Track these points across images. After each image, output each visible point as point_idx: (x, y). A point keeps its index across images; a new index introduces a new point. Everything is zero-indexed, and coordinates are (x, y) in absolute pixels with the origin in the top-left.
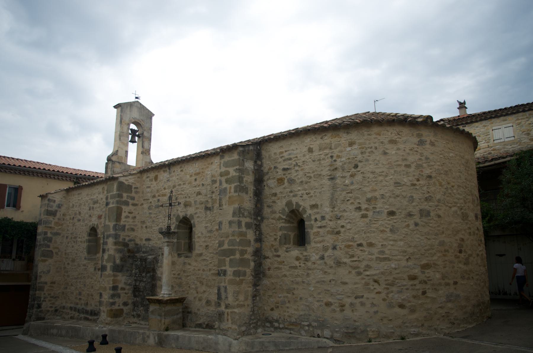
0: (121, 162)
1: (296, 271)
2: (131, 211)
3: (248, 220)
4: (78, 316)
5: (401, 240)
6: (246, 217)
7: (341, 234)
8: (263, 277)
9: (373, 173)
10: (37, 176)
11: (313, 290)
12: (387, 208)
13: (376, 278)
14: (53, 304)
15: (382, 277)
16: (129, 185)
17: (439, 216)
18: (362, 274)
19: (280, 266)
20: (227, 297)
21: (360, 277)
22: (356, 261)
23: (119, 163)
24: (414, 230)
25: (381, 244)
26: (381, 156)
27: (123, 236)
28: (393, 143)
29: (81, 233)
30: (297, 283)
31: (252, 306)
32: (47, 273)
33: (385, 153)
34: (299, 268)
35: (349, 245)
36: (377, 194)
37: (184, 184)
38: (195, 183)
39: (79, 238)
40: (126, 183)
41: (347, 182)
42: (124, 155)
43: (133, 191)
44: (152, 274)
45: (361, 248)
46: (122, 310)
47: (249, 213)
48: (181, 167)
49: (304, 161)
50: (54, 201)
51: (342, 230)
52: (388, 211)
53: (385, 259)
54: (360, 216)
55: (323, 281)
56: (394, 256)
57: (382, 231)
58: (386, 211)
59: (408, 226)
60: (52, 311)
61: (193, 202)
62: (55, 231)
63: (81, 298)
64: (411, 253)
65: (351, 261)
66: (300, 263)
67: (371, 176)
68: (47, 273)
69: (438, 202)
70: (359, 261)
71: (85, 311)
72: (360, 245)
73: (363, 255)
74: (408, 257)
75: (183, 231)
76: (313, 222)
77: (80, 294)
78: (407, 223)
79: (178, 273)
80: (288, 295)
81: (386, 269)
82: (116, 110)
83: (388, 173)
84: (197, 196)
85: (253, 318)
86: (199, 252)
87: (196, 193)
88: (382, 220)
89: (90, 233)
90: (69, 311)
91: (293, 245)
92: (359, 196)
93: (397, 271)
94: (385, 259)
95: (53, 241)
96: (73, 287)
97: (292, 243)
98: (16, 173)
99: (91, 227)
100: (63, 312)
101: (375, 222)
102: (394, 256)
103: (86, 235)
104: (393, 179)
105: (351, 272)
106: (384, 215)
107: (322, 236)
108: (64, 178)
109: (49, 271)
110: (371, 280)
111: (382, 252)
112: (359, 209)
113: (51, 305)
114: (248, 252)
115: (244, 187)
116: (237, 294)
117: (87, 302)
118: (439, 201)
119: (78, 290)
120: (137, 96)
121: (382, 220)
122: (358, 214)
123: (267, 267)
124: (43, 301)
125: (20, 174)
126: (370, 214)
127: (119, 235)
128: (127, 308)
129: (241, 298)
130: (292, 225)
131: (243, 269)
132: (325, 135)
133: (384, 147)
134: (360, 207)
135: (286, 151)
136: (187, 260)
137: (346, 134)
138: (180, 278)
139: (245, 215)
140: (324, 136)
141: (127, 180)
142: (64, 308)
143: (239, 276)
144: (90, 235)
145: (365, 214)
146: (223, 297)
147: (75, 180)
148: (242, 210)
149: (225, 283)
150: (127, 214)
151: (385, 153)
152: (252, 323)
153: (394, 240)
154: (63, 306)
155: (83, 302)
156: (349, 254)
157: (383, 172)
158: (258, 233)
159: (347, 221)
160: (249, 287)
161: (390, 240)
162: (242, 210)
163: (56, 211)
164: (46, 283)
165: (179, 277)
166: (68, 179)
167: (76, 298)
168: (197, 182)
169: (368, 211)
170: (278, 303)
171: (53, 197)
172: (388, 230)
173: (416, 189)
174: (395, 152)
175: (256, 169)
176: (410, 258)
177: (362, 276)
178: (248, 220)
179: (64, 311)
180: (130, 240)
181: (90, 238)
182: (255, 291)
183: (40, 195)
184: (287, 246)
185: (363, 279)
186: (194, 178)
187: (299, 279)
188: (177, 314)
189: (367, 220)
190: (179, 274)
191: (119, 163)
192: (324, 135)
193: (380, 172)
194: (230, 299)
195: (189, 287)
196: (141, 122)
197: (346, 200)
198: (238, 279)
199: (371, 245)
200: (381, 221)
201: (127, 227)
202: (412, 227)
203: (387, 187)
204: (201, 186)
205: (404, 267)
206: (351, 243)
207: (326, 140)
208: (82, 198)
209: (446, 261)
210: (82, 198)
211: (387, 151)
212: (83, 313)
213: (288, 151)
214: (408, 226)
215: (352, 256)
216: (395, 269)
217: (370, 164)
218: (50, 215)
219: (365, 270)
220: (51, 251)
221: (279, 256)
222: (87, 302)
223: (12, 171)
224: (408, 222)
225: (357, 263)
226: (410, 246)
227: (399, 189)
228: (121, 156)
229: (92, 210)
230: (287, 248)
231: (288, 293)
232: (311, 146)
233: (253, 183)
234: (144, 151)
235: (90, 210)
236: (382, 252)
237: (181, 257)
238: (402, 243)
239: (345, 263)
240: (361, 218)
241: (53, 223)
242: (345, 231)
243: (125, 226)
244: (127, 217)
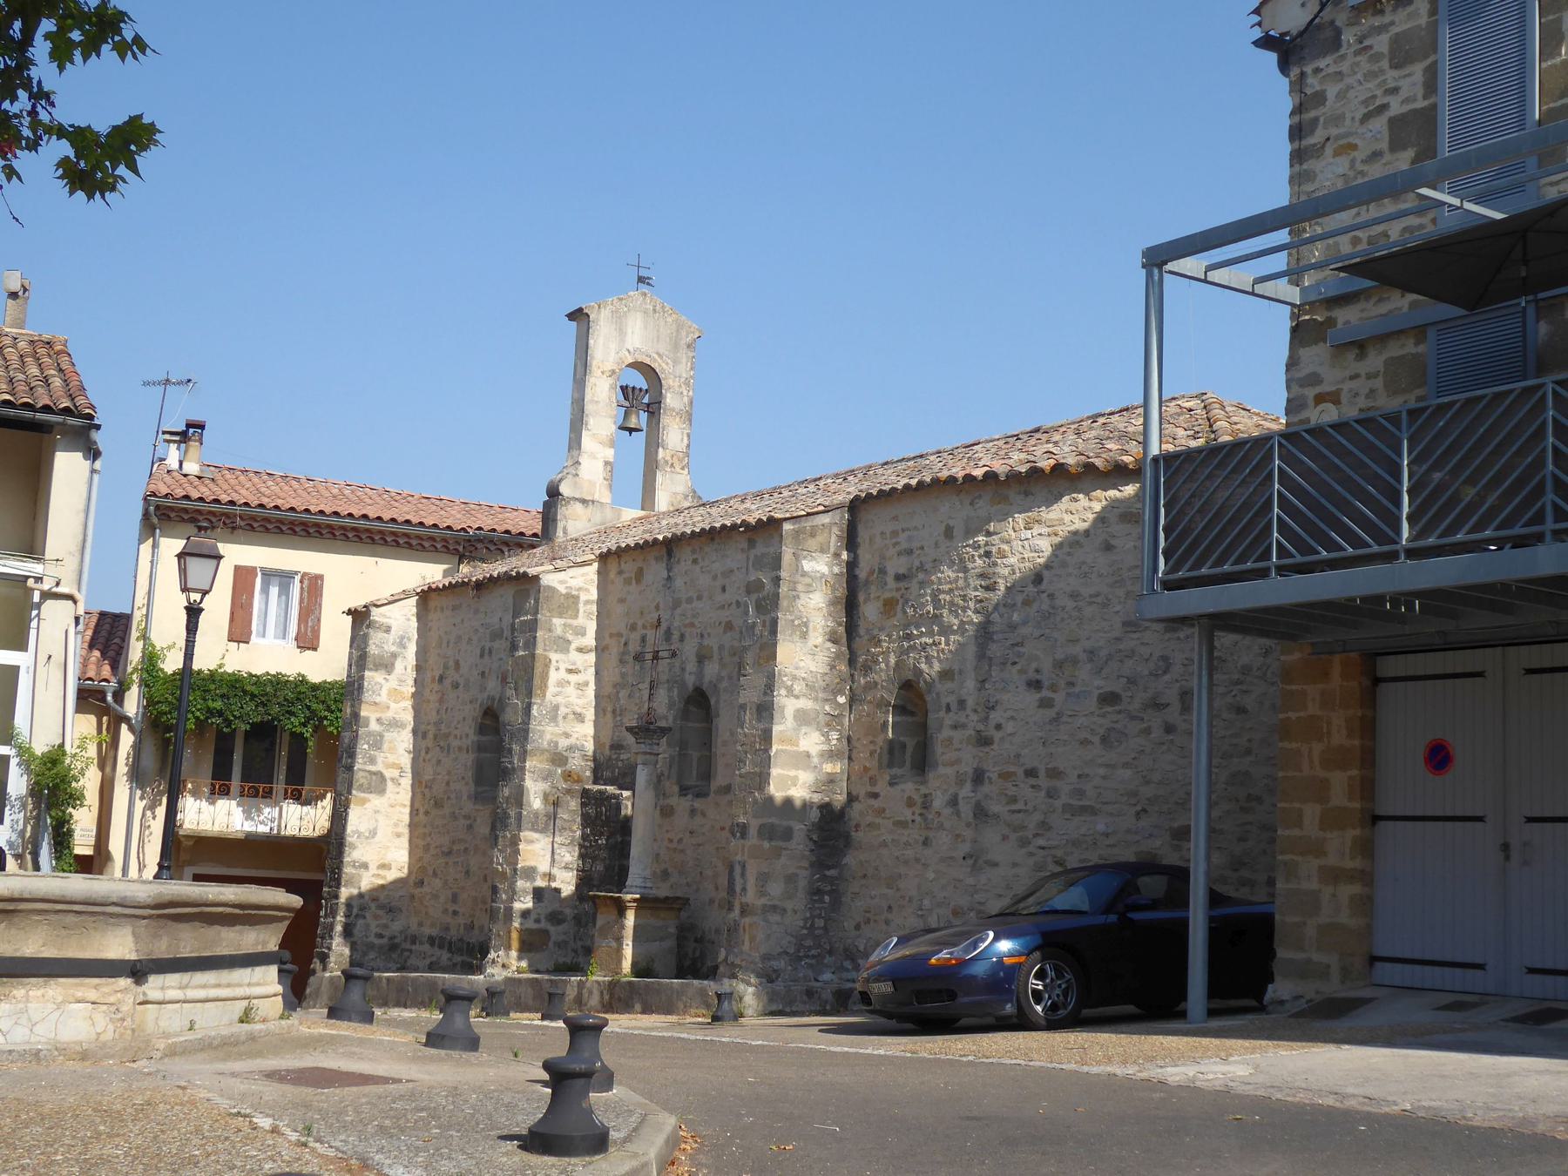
0: (590, 498)
1: (906, 832)
2: (573, 667)
3: (805, 704)
4: (450, 959)
5: (1126, 765)
6: (797, 697)
7: (995, 746)
8: (845, 846)
9: (1074, 596)
10: (343, 537)
11: (934, 879)
12: (1100, 684)
13: (1059, 853)
14: (386, 926)
15: (1072, 853)
16: (568, 596)
17: (1241, 710)
18: (1030, 843)
19: (877, 820)
20: (744, 889)
21: (1024, 851)
22: (1019, 811)
23: (584, 502)
24: (1163, 744)
25: (1076, 773)
26: (1097, 555)
27: (552, 734)
28: (1130, 521)
29: (459, 722)
30: (906, 862)
31: (808, 915)
32: (367, 838)
33: (1108, 547)
34: (910, 825)
35: (1008, 772)
36: (1076, 650)
37: (700, 598)
38: (720, 598)
39: (456, 736)
40: (562, 589)
41: (1016, 617)
42: (601, 477)
43: (581, 611)
44: (620, 839)
45: (1032, 781)
46: (545, 932)
47: (807, 685)
48: (694, 551)
49: (935, 560)
50: (388, 630)
51: (997, 735)
52: (1101, 694)
53: (1084, 810)
54: (1037, 704)
55: (951, 858)
56: (1106, 803)
57: (1085, 742)
58: (1097, 693)
59: (1147, 731)
60: (381, 947)
61: (715, 649)
62: (389, 715)
63: (457, 909)
64: (1148, 799)
65: (1009, 811)
66: (913, 814)
67: (1070, 604)
68: (367, 838)
69: (1244, 674)
70: (1026, 811)
71: (465, 947)
72: (1031, 773)
73: (1036, 797)
74: (1139, 808)
75: (697, 725)
76: (942, 714)
77: (455, 898)
78: (1145, 725)
79: (678, 837)
80: (889, 891)
81: (1084, 835)
82: (574, 324)
83: (1110, 597)
84: (725, 632)
85: (808, 943)
86: (724, 784)
87: (723, 624)
88: (1086, 715)
89: (481, 724)
90: (426, 947)
91: (912, 769)
92: (1038, 653)
93: (1111, 841)
94: (1084, 810)
95: (385, 746)
96: (437, 880)
97: (908, 764)
98: (282, 532)
99: (485, 707)
100: (411, 951)
101: (1070, 720)
102: (1106, 803)
103: (472, 731)
104: (1121, 614)
105: (1008, 837)
106: (1091, 704)
107: (956, 750)
108: (426, 544)
109: (373, 833)
110: (1049, 859)
111: (1080, 793)
112: (1035, 685)
113: (379, 931)
114: (801, 782)
115: (796, 623)
116: (763, 878)
117: (472, 922)
118: (1246, 670)
119: (451, 888)
120: (643, 273)
121: (1086, 715)
122: (1033, 698)
123: (853, 823)
124: (357, 916)
125: (295, 533)
126: (1059, 698)
127: (539, 731)
128: (561, 928)
129: (776, 889)
130: (910, 719)
131: (785, 823)
132: (980, 497)
133: (1107, 532)
134: (1038, 682)
135: (903, 530)
136: (698, 804)
137: (1022, 497)
138: (682, 851)
139: (796, 692)
140: (976, 498)
141: (562, 582)
142: (414, 940)
143: (771, 839)
144: (482, 730)
145: (1049, 698)
146: (738, 889)
147: (461, 549)
148: (785, 679)
149: (743, 855)
150: (562, 674)
151: (1108, 547)
152: (807, 957)
153: (1107, 766)
154: (412, 936)
155: (462, 922)
156: (1006, 795)
157: (1097, 595)
158: (836, 737)
159: (1009, 713)
160: (800, 867)
161: (1101, 765)
162: (785, 679)
163: (394, 656)
164: (365, 866)
165: (680, 847)
166: (439, 546)
167: (445, 911)
168: (727, 596)
169: (1055, 691)
170: (869, 912)
171: (385, 616)
172: (1096, 740)
173: (1179, 639)
174: (1132, 544)
175: (837, 574)
176: (1144, 810)
177: (1031, 848)
178: (805, 704)
179: (414, 947)
180: (570, 748)
181: (484, 738)
182: (819, 880)
183: (349, 610)
184: (895, 771)
185: (1031, 854)
186: (719, 583)
187: (909, 853)
188: (662, 939)
189: (1051, 713)
190: (680, 841)
191: (584, 502)
192: (977, 494)
193: (1091, 596)
194: (750, 897)
195: (701, 873)
196: (655, 360)
197: (1010, 662)
198: (766, 845)
199: (1055, 774)
200: (1084, 718)
201: (563, 711)
202: (1157, 733)
203: (1105, 632)
204: (734, 606)
205: (1128, 831)
206: (1012, 769)
207: (980, 508)
208: (463, 621)
209: (1251, 823)
210: (463, 621)
211: (1113, 542)
212: (460, 951)
213: (908, 529)
214: (1147, 731)
215: (1014, 800)
216: (1107, 835)
217: (1070, 575)
218: (376, 670)
219: (1036, 835)
220: (380, 775)
221: (875, 796)
222: (472, 922)
223: (270, 526)
224: (1150, 720)
225: (1020, 815)
226: (1148, 783)
227: (1133, 639)
228: (590, 481)
229: (486, 657)
230: (893, 777)
231: (889, 887)
232: (951, 523)
233: (825, 610)
234: (668, 458)
235: (482, 656)
236: (1080, 793)
237: (685, 795)
238: (1127, 773)
239: (997, 816)
240: (1039, 707)
241: (384, 692)
242: (1002, 739)
243: (556, 708)
244: (562, 684)
